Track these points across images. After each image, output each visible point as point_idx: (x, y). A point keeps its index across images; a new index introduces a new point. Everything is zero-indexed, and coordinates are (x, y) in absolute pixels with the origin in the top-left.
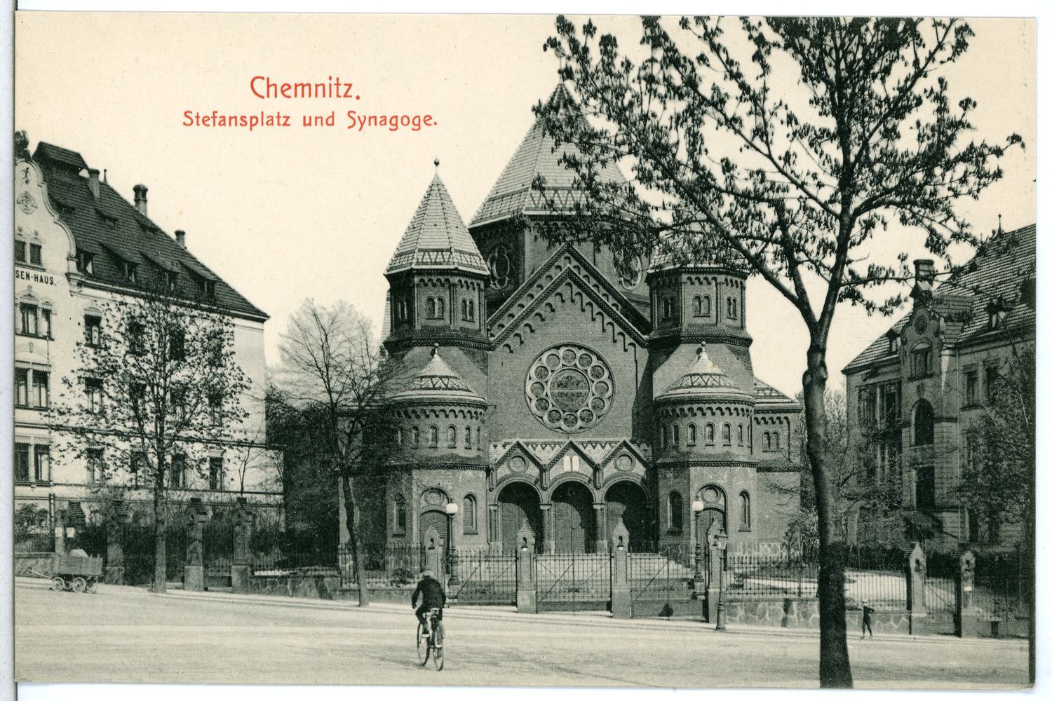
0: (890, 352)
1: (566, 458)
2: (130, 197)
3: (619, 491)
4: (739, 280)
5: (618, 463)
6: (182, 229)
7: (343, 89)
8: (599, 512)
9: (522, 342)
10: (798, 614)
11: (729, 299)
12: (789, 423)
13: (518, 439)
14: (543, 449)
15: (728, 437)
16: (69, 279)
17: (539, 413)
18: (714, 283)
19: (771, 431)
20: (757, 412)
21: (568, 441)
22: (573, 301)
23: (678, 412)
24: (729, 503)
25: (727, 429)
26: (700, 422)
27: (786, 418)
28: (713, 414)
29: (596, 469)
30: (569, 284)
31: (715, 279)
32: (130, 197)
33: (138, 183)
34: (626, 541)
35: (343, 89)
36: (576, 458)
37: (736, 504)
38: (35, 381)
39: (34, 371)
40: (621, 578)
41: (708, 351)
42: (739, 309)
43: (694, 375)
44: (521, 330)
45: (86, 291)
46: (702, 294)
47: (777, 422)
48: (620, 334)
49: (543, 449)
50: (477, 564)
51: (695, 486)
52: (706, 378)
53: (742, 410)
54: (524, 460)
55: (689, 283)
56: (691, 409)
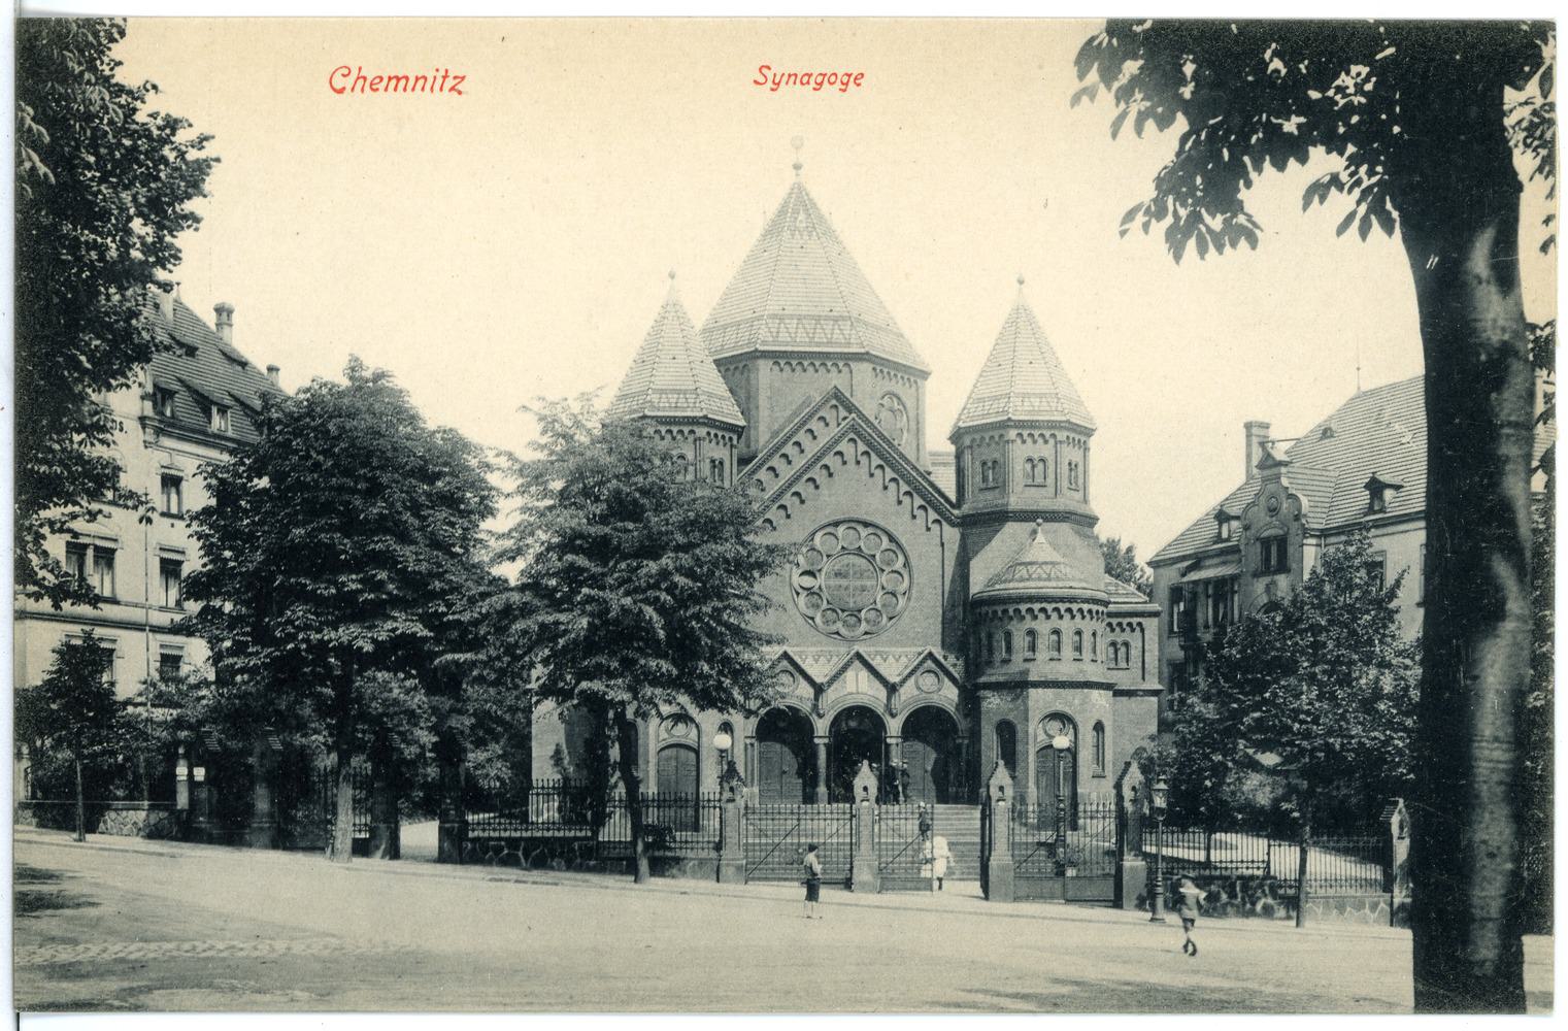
0: (1219, 539)
1: (850, 674)
2: (210, 319)
3: (925, 723)
4: (1083, 439)
5: (921, 681)
6: (276, 364)
7: (450, 82)
8: (893, 748)
9: (788, 516)
10: (1243, 899)
11: (1070, 464)
12: (1142, 630)
13: (785, 648)
14: (817, 661)
15: (1079, 649)
16: (144, 427)
17: (810, 613)
18: (1052, 441)
19: (1119, 640)
20: (1110, 615)
21: (781, 652)
22: (858, 463)
23: (1011, 613)
24: (1080, 737)
25: (1077, 638)
26: (1043, 627)
27: (1140, 624)
28: (1061, 617)
29: (892, 689)
30: (851, 440)
31: (1053, 436)
32: (210, 319)
33: (218, 301)
34: (873, 791)
35: (450, 82)
36: (864, 674)
37: (1087, 736)
38: (96, 563)
39: (97, 548)
40: (865, 847)
41: (1045, 532)
42: (1081, 476)
43: (1031, 563)
44: (787, 500)
45: (167, 442)
46: (1036, 457)
47: (1128, 629)
48: (921, 507)
49: (817, 661)
50: (795, 822)
51: (1035, 716)
52: (1047, 568)
53: (1090, 611)
54: (937, 675)
55: (1019, 441)
56: (1018, 611)
